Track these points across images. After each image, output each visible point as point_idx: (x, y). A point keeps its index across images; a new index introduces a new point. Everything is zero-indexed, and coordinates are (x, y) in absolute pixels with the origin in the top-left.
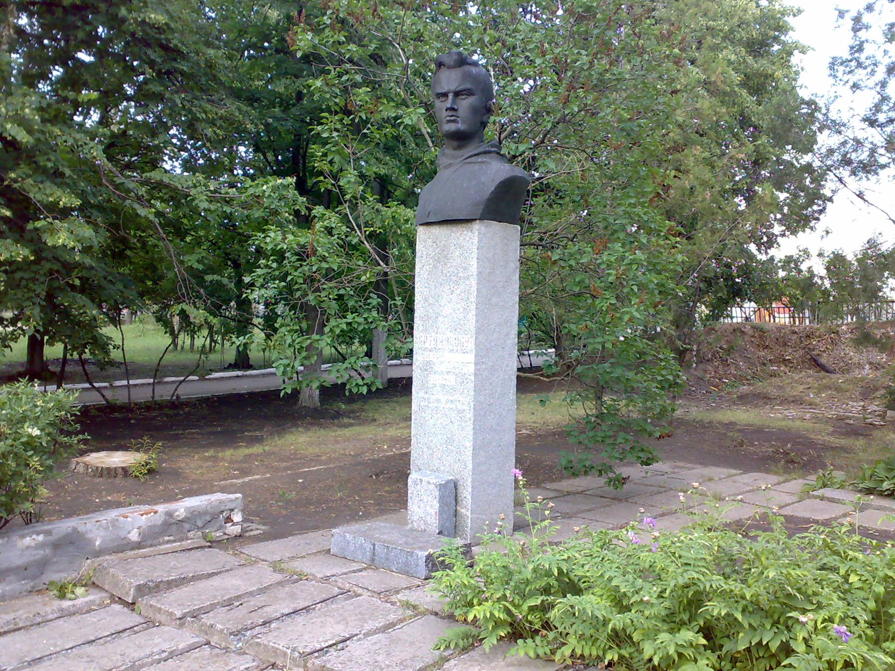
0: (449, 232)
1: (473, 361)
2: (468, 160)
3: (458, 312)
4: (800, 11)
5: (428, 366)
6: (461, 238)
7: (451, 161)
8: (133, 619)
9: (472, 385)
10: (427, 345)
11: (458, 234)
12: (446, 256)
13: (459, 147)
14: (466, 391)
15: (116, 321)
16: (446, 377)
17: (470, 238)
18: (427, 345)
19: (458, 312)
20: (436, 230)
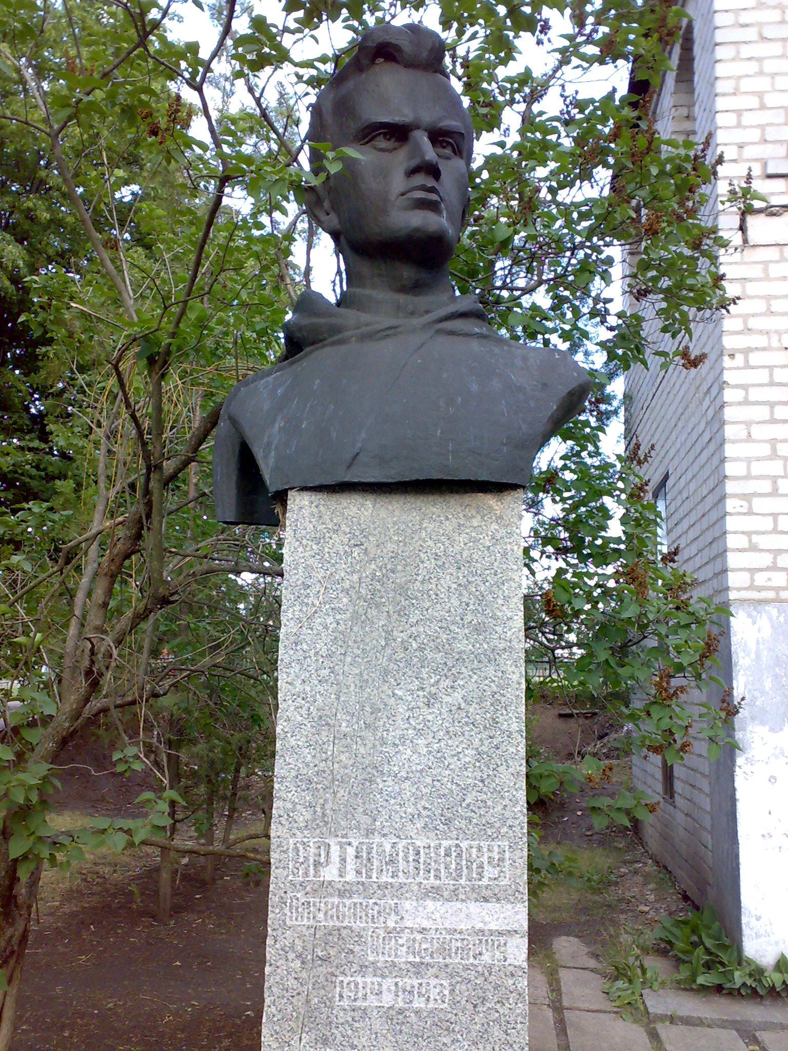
0: (415, 516)
1: (523, 924)
2: (449, 325)
3: (455, 764)
4: (561, 36)
5: (332, 951)
6: (463, 538)
7: (392, 322)
8: (755, 538)
9: (523, 1008)
10: (330, 873)
11: (449, 526)
12: (402, 590)
13: (416, 288)
14: (496, 1032)
15: (548, 291)
16: (410, 982)
17: (496, 540)
18: (330, 873)
19: (455, 764)
20: (360, 510)
